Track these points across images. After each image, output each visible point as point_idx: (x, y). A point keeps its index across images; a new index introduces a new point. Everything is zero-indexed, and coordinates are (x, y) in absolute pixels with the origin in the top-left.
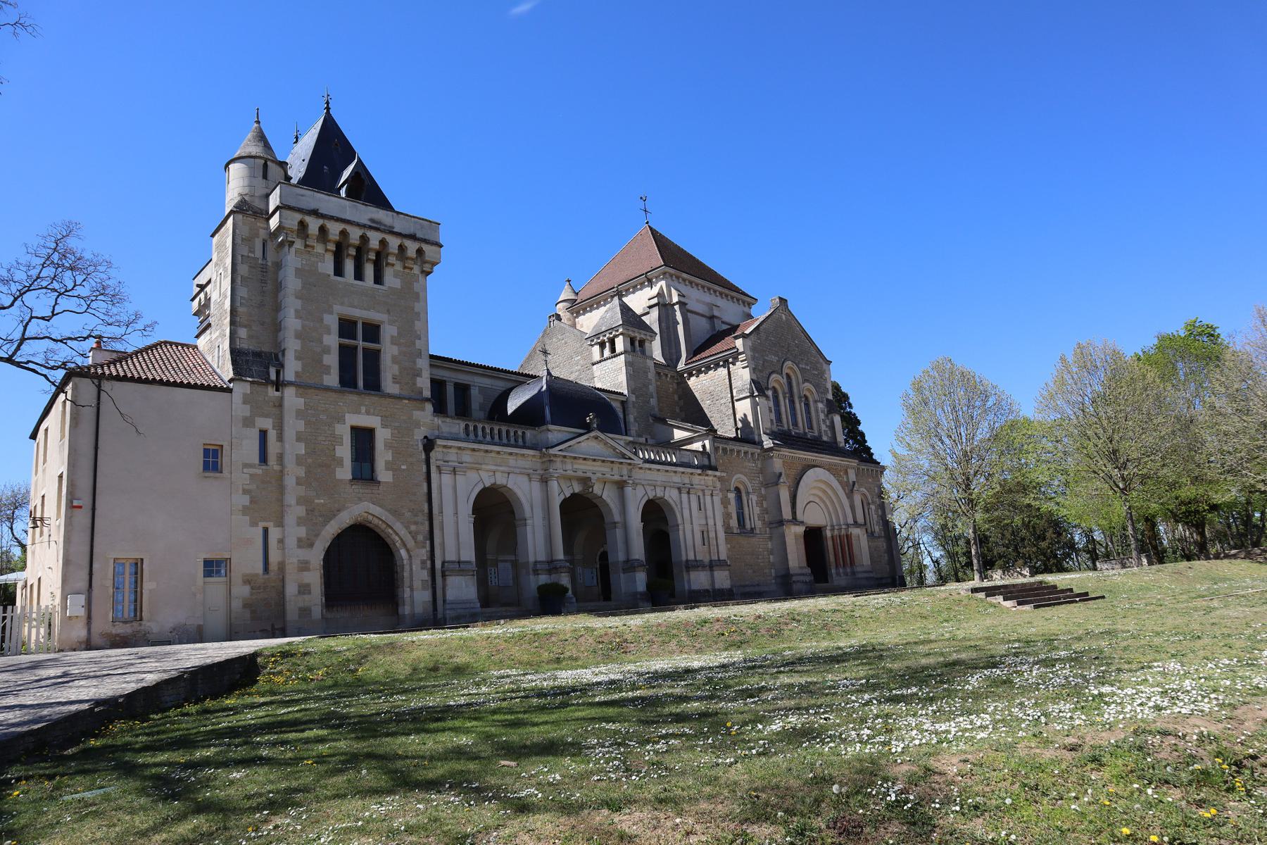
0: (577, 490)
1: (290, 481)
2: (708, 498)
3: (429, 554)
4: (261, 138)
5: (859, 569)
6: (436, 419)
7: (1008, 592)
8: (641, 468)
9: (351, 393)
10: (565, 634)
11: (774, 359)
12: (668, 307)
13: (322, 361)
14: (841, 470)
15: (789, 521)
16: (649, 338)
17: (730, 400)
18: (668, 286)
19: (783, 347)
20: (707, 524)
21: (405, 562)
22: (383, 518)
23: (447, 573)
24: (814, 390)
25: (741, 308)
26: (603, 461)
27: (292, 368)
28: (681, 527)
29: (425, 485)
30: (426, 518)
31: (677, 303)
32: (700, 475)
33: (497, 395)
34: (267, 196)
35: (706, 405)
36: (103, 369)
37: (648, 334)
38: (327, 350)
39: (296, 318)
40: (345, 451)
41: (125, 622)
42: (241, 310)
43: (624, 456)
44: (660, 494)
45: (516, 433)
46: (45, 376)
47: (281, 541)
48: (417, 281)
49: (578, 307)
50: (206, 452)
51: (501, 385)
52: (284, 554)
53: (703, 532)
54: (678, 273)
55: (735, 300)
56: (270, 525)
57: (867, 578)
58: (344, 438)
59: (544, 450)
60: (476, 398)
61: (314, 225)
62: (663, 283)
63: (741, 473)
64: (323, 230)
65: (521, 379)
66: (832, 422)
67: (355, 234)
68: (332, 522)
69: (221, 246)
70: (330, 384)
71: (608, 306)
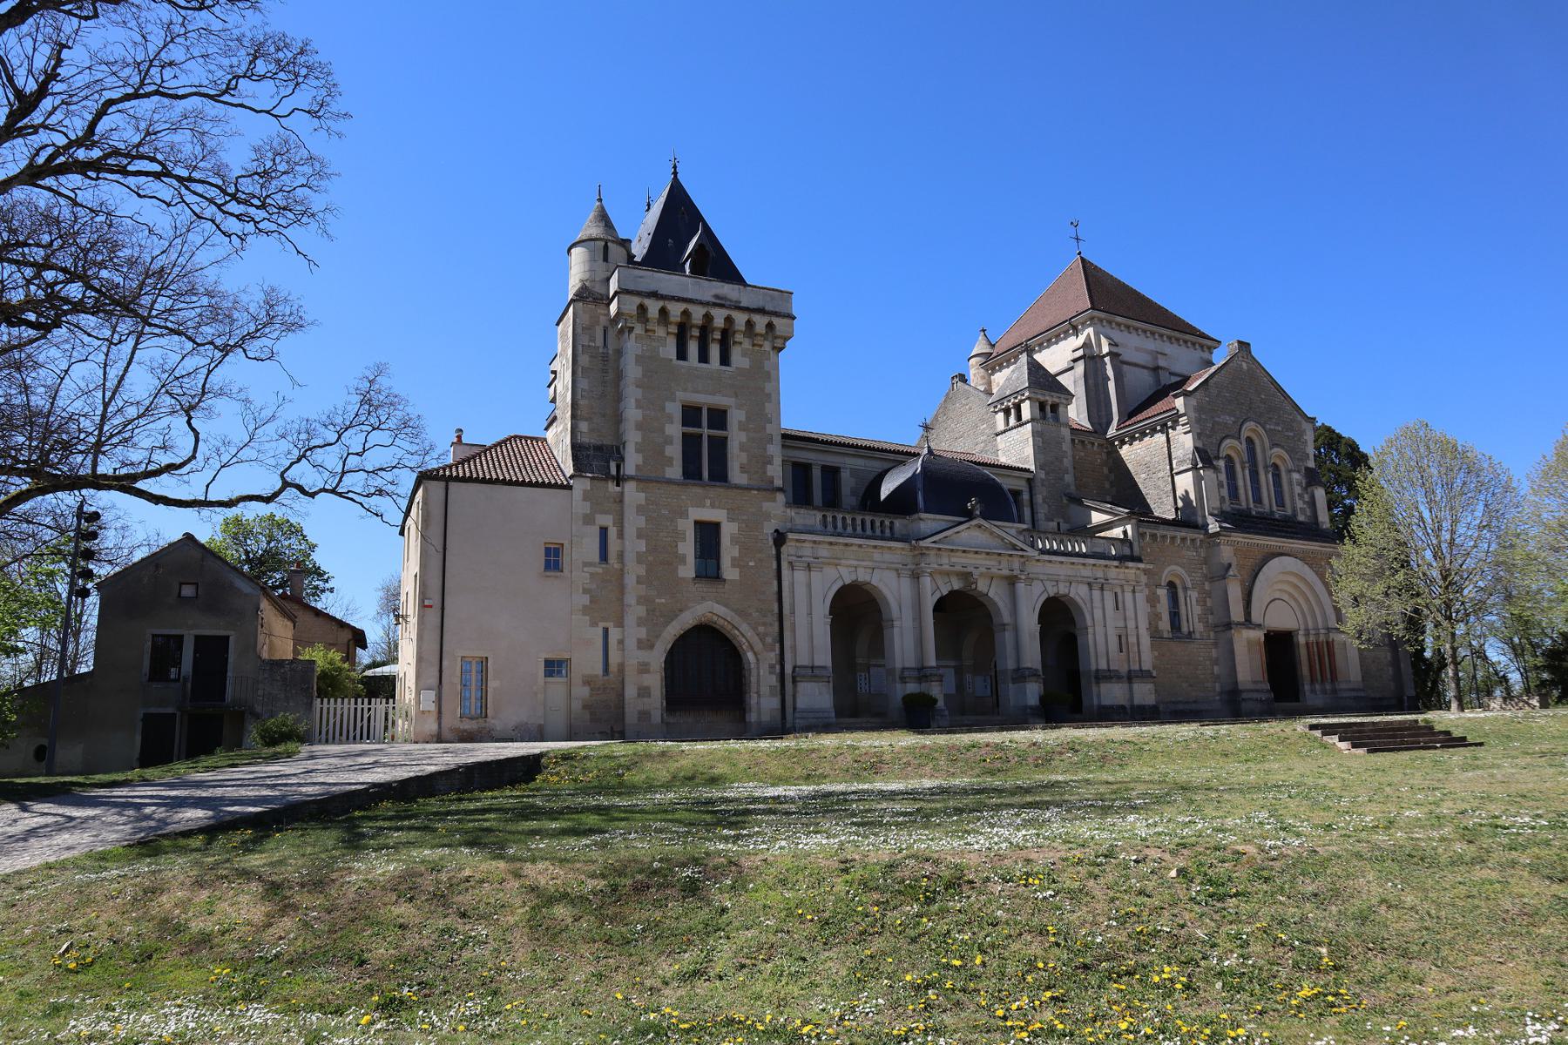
0: (956, 587)
1: (630, 580)
2: (1128, 596)
3: (778, 657)
4: (604, 218)
5: (1343, 686)
6: (788, 510)
7: (1345, 733)
8: (1038, 560)
9: (694, 485)
10: (827, 751)
11: (1229, 420)
12: (1097, 359)
13: (664, 452)
14: (1322, 559)
15: (1239, 624)
16: (1064, 401)
17: (1169, 474)
19: (1242, 404)
20: (1126, 627)
21: (752, 666)
22: (729, 619)
23: (798, 679)
24: (1286, 456)
25: (1198, 354)
26: (988, 554)
28: (1090, 630)
30: (776, 618)
31: (1107, 354)
32: (1117, 567)
33: (871, 477)
34: (608, 279)
35: (1140, 479)
36: (451, 471)
37: (1063, 396)
38: (669, 440)
39: (637, 408)
40: (688, 548)
41: (471, 719)
42: (582, 402)
43: (1014, 547)
44: (1063, 589)
45: (882, 523)
46: (361, 504)
47: (621, 642)
48: (768, 359)
49: (992, 363)
50: (548, 551)
51: (877, 466)
52: (624, 656)
53: (1120, 636)
54: (1111, 317)
55: (1189, 344)
56: (610, 625)
57: (1355, 698)
58: (687, 534)
59: (914, 542)
60: (847, 482)
62: (1090, 330)
63: (1177, 564)
64: (663, 312)
65: (900, 457)
66: (1313, 497)
67: (698, 313)
68: (674, 623)
69: (564, 334)
70: (673, 477)
71: (1012, 368)
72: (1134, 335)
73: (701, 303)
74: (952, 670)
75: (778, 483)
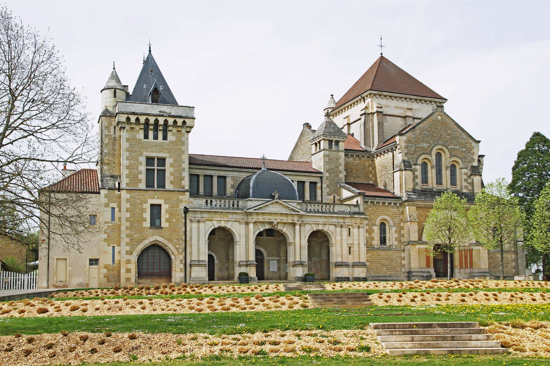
1: (123, 228)
5: (475, 271)
6: (191, 199)
18: (372, 102)
19: (435, 137)
27: (124, 181)
29: (184, 228)
30: (184, 242)
38: (140, 173)
40: (147, 215)
47: (119, 252)
53: (350, 248)
56: (115, 245)
61: (133, 119)
64: (138, 120)
67: (152, 120)
68: (141, 244)
72: (395, 100)
73: (154, 115)
74: (276, 262)
75: (187, 188)
